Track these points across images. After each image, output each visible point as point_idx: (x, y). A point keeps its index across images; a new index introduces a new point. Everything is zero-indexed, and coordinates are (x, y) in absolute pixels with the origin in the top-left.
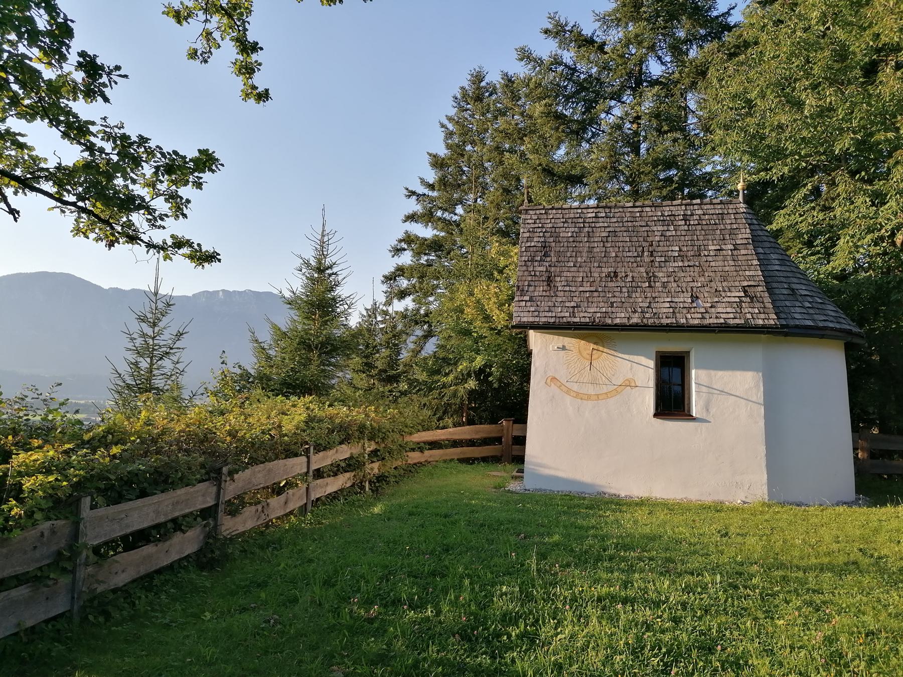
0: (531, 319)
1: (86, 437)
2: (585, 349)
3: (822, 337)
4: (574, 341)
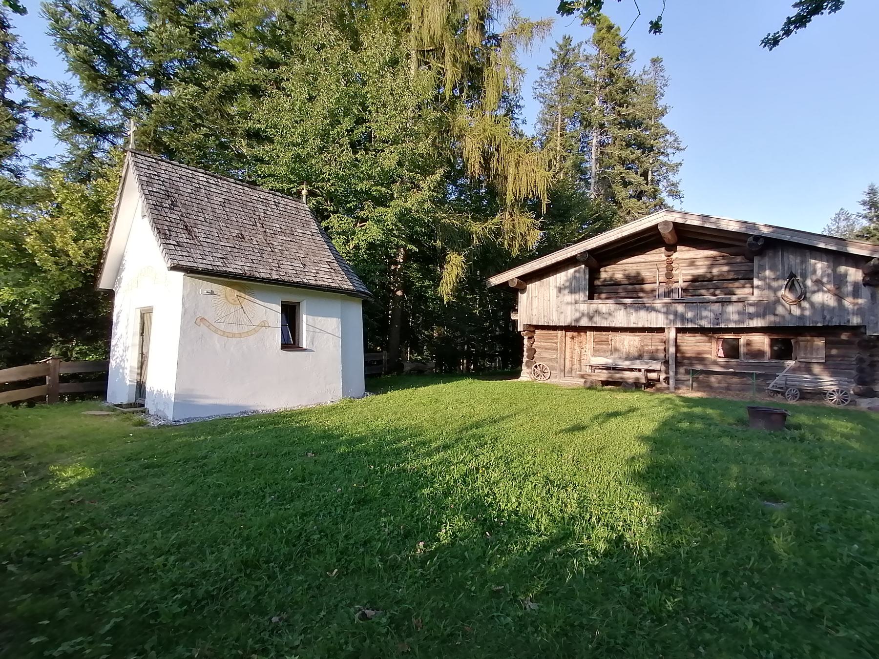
0: (189, 264)
1: (447, 91)
2: (230, 296)
3: (818, 254)
4: (221, 287)
